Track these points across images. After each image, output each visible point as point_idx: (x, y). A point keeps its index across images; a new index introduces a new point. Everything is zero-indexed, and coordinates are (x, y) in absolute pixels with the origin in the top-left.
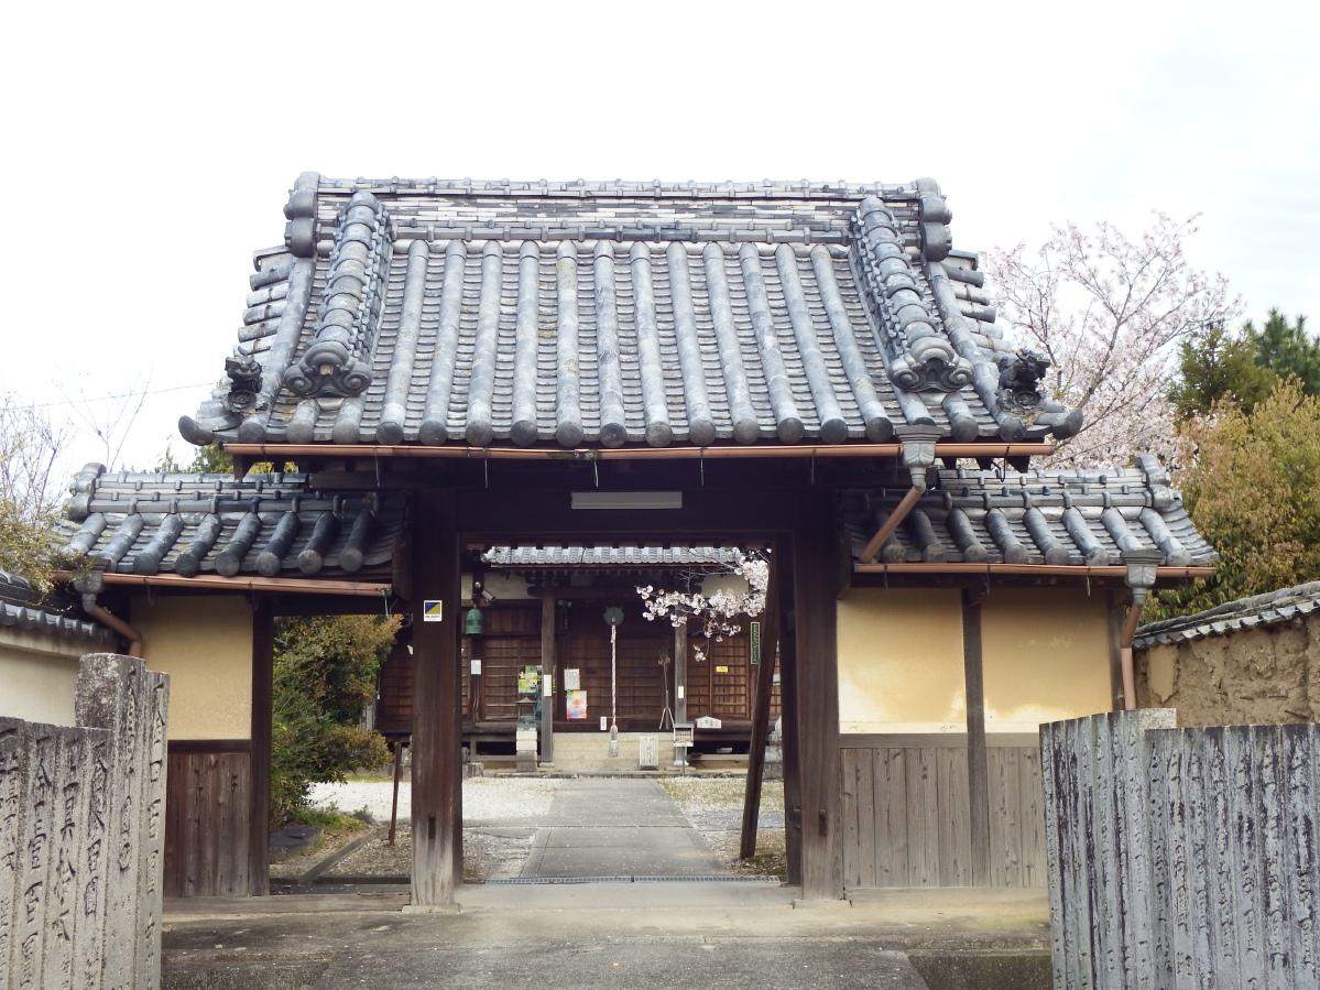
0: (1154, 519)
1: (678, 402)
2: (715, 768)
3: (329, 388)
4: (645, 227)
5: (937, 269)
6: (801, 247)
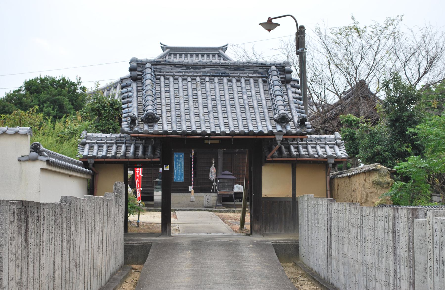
0: (336, 148)
1: (227, 124)
2: (137, 236)
3: (150, 121)
4: (217, 73)
5: (289, 86)
6: (255, 78)
